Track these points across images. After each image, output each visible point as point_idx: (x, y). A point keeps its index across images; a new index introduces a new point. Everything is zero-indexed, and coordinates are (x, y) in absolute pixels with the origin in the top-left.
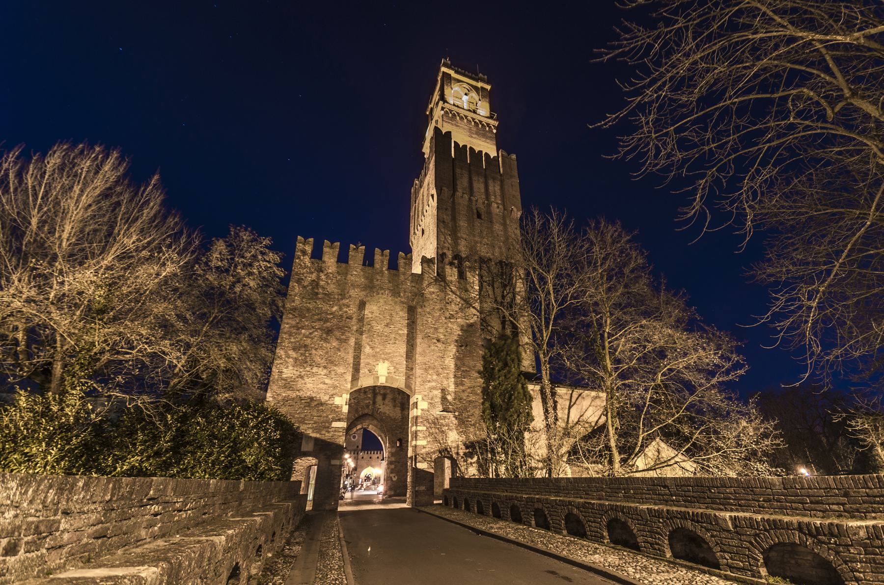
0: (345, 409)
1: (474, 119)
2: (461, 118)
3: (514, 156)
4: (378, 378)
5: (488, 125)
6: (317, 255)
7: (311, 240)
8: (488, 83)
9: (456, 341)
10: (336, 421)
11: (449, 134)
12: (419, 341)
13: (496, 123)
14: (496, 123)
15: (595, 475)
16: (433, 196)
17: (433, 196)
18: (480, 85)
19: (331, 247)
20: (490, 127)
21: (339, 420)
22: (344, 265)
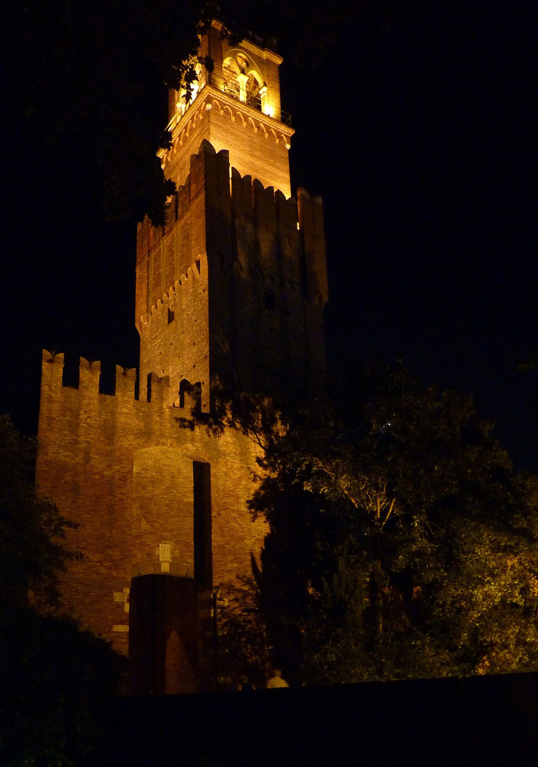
0: (127, 608)
1: (257, 123)
2: (238, 118)
3: (319, 200)
4: (160, 565)
5: (279, 134)
6: (71, 379)
7: (61, 355)
8: (277, 51)
9: (248, 502)
10: (117, 624)
11: (224, 153)
12: (190, 499)
13: (291, 132)
14: (291, 132)
15: (393, 679)
16: (198, 263)
17: (198, 263)
18: (265, 55)
19: (90, 368)
20: (281, 138)
21: (122, 623)
22: (108, 397)
